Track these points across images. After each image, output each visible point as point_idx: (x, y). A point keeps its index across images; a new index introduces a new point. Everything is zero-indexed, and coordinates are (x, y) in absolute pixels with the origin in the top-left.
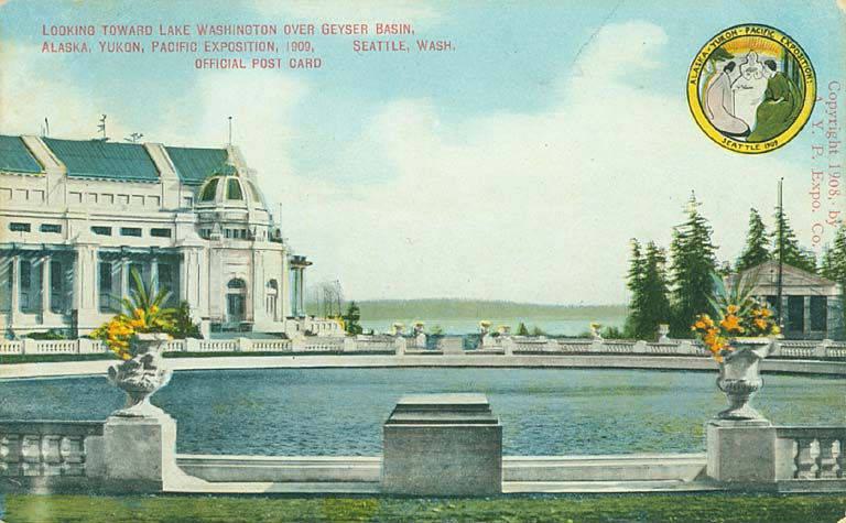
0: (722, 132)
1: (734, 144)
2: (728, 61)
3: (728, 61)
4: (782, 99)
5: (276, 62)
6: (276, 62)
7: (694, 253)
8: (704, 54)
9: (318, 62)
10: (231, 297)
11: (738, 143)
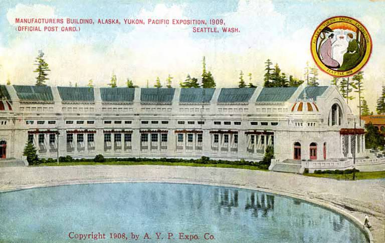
0: (326, 65)
1: (332, 72)
2: (330, 33)
3: (330, 33)
4: (355, 51)
5: (55, 29)
6: (55, 29)
7: (47, 65)
8: (320, 30)
9: (74, 29)
10: (311, 150)
11: (334, 71)
